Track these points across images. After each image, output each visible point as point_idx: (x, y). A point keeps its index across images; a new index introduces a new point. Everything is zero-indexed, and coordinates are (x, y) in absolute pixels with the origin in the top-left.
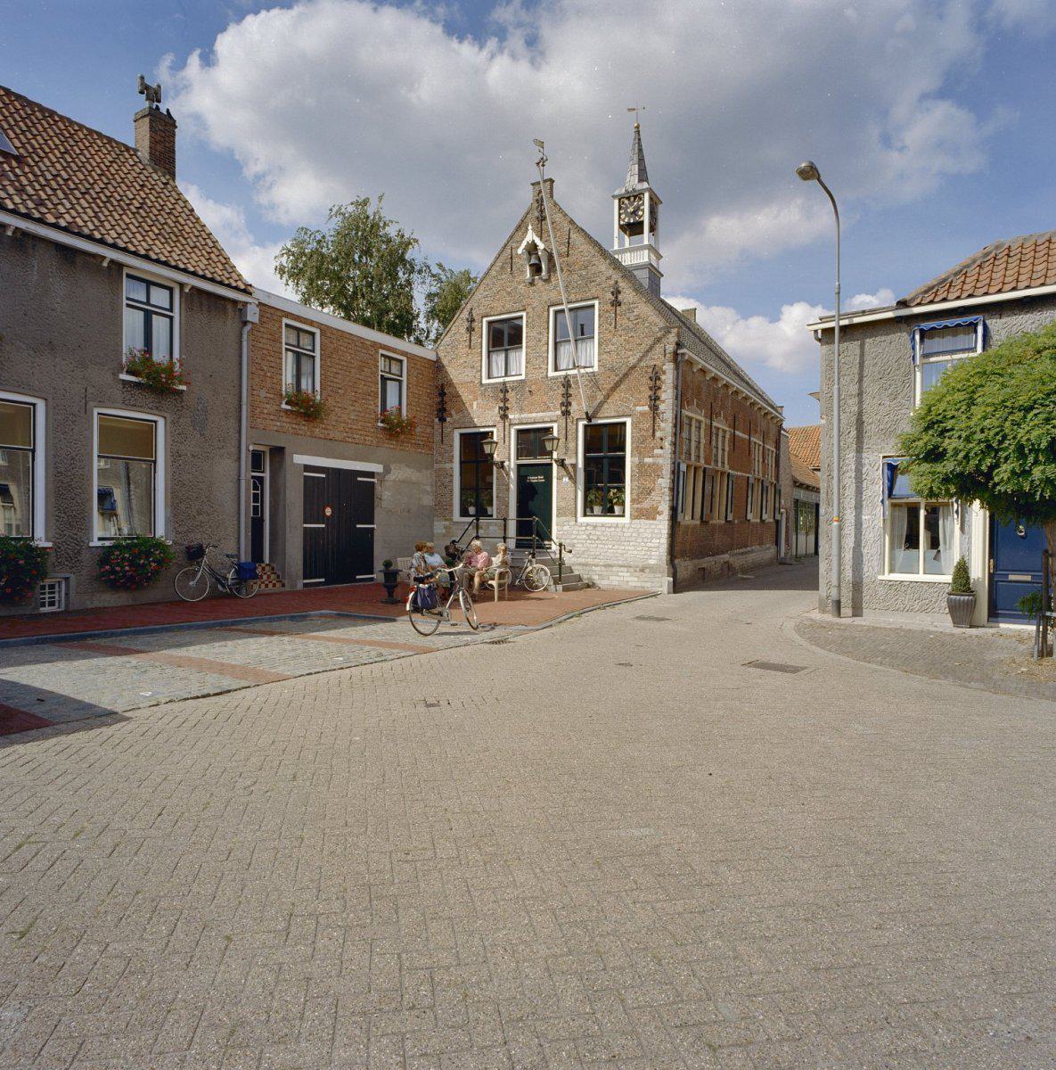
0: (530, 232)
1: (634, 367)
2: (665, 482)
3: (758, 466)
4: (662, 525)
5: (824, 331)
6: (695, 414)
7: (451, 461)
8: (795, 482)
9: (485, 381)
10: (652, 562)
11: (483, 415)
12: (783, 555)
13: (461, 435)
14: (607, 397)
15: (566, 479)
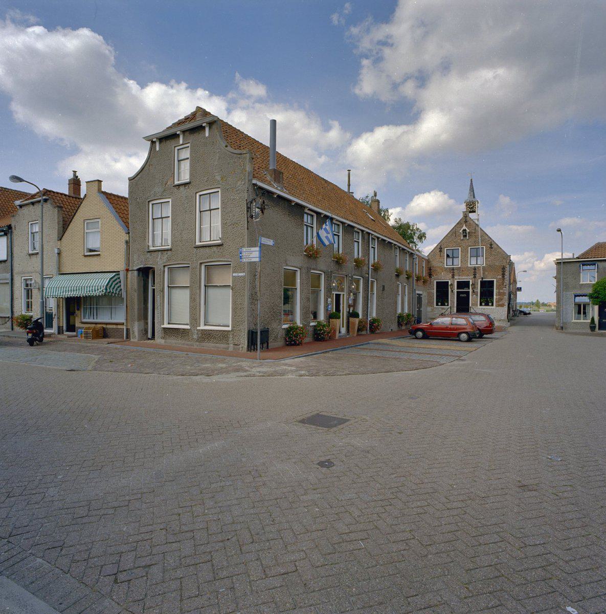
4: (506, 308)
9: (445, 266)
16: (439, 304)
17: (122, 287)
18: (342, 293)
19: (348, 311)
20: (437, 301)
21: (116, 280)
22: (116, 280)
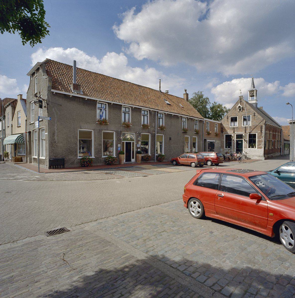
0: (239, 104)
1: (257, 125)
2: (263, 143)
3: (277, 138)
4: (263, 149)
5: (290, 123)
6: (268, 132)
7: (224, 139)
8: (284, 140)
9: (230, 127)
10: (261, 155)
11: (230, 132)
12: (282, 154)
13: (226, 135)
14: (253, 130)
15: (245, 142)
16: (227, 147)
17: (24, 140)
18: (132, 142)
19: (136, 150)
20: (226, 146)
21: (22, 137)
22: (22, 137)
